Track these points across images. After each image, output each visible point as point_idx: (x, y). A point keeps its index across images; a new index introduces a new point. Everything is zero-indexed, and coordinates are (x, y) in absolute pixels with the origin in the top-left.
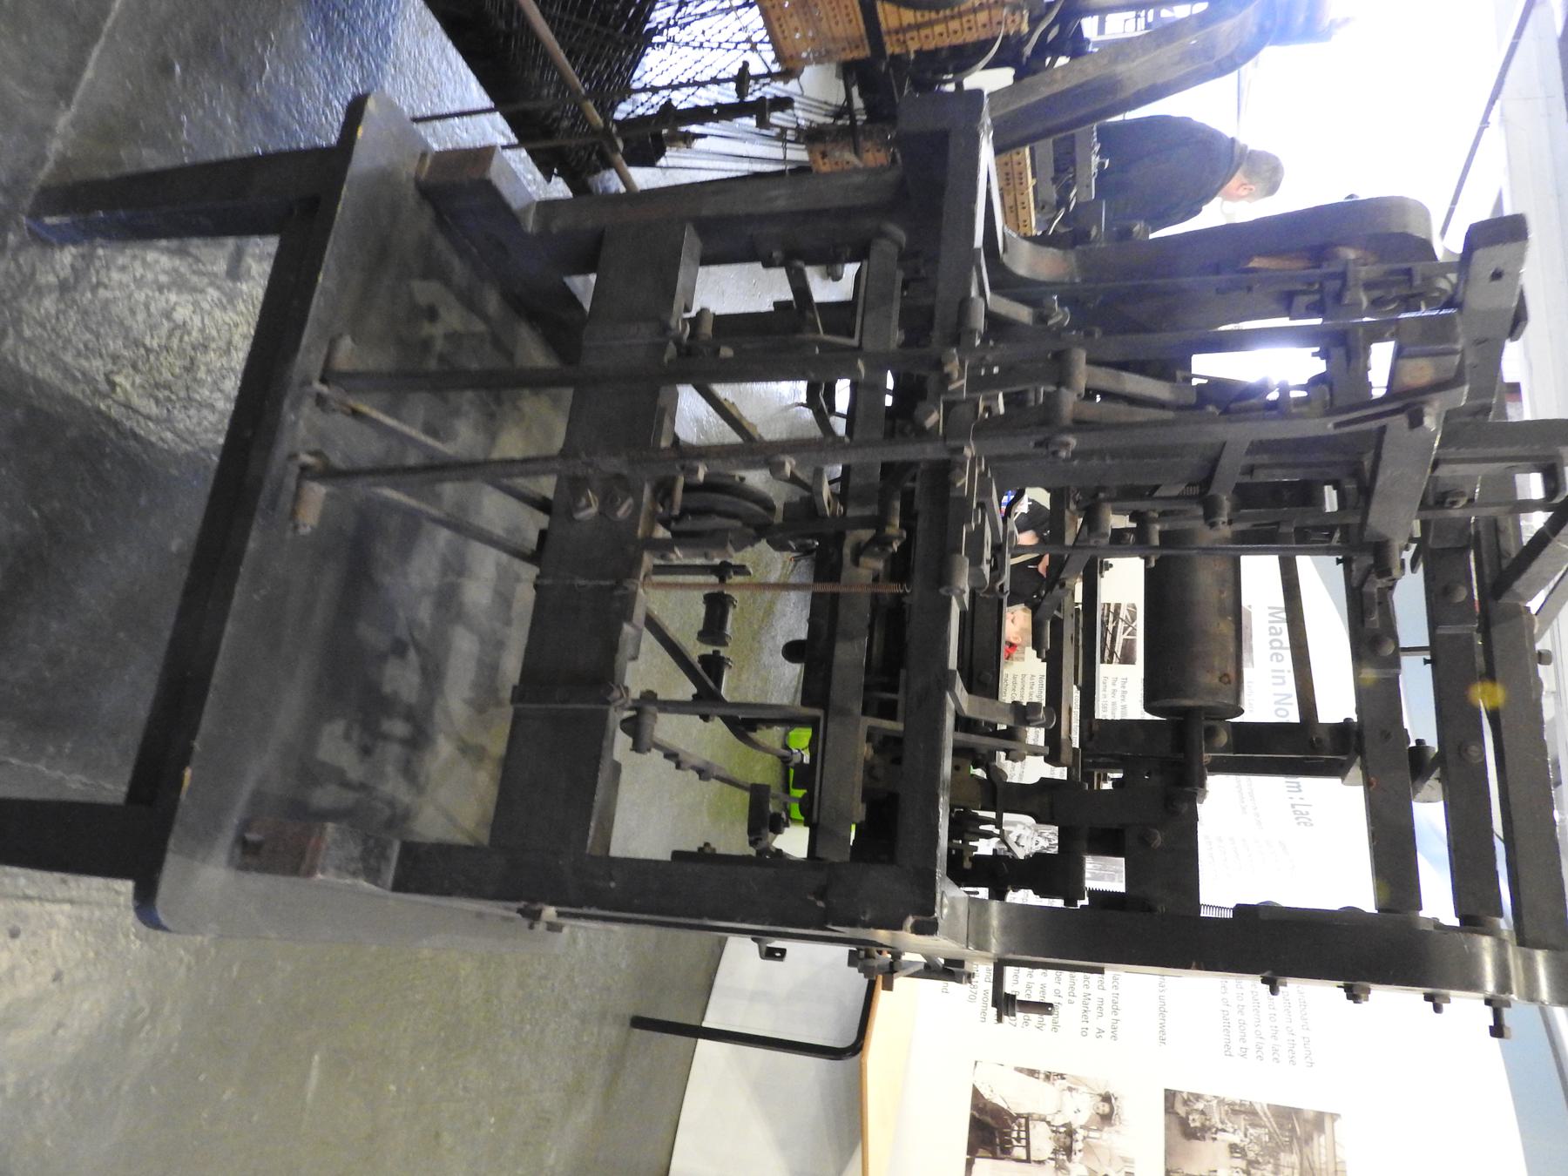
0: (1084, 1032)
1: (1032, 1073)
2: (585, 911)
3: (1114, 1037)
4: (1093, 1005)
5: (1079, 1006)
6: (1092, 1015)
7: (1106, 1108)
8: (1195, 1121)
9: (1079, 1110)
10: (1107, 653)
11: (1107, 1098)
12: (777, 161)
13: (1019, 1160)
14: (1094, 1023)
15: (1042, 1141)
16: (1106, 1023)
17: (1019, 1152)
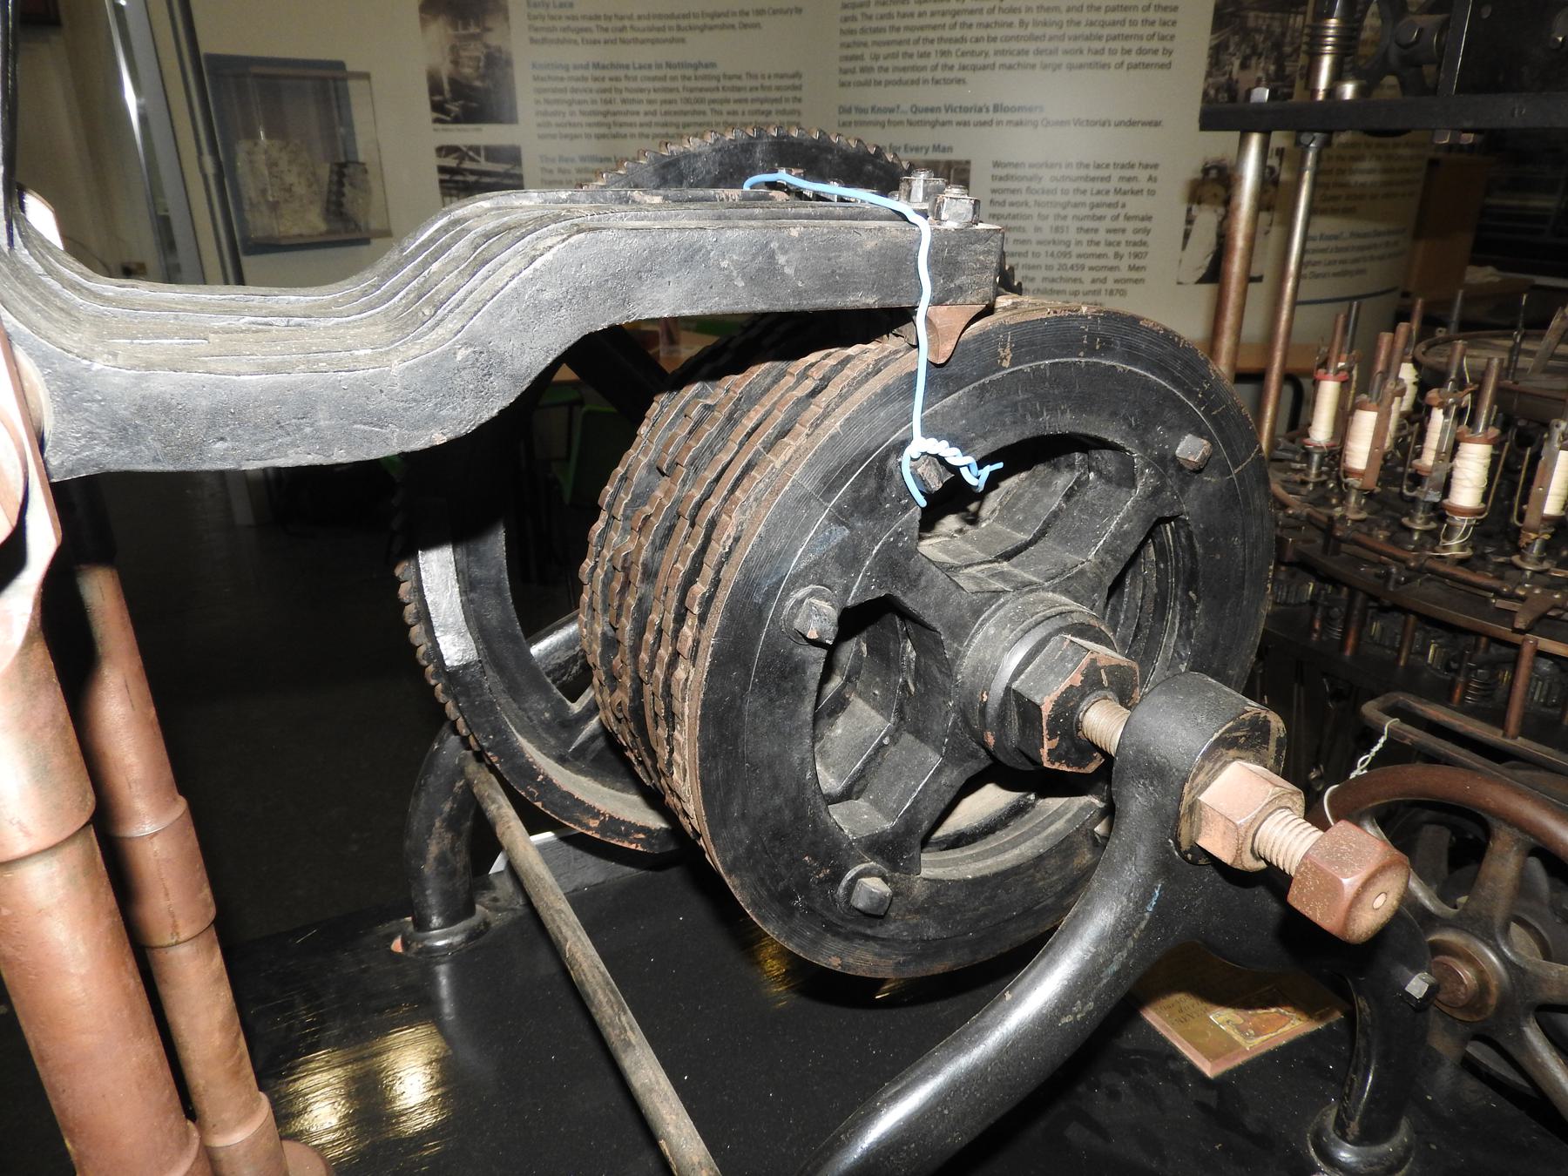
0: (1152, 193)
1: (1187, 235)
3: (1156, 166)
4: (1126, 186)
5: (1129, 199)
6: (1135, 186)
14: (1143, 184)
16: (1143, 175)
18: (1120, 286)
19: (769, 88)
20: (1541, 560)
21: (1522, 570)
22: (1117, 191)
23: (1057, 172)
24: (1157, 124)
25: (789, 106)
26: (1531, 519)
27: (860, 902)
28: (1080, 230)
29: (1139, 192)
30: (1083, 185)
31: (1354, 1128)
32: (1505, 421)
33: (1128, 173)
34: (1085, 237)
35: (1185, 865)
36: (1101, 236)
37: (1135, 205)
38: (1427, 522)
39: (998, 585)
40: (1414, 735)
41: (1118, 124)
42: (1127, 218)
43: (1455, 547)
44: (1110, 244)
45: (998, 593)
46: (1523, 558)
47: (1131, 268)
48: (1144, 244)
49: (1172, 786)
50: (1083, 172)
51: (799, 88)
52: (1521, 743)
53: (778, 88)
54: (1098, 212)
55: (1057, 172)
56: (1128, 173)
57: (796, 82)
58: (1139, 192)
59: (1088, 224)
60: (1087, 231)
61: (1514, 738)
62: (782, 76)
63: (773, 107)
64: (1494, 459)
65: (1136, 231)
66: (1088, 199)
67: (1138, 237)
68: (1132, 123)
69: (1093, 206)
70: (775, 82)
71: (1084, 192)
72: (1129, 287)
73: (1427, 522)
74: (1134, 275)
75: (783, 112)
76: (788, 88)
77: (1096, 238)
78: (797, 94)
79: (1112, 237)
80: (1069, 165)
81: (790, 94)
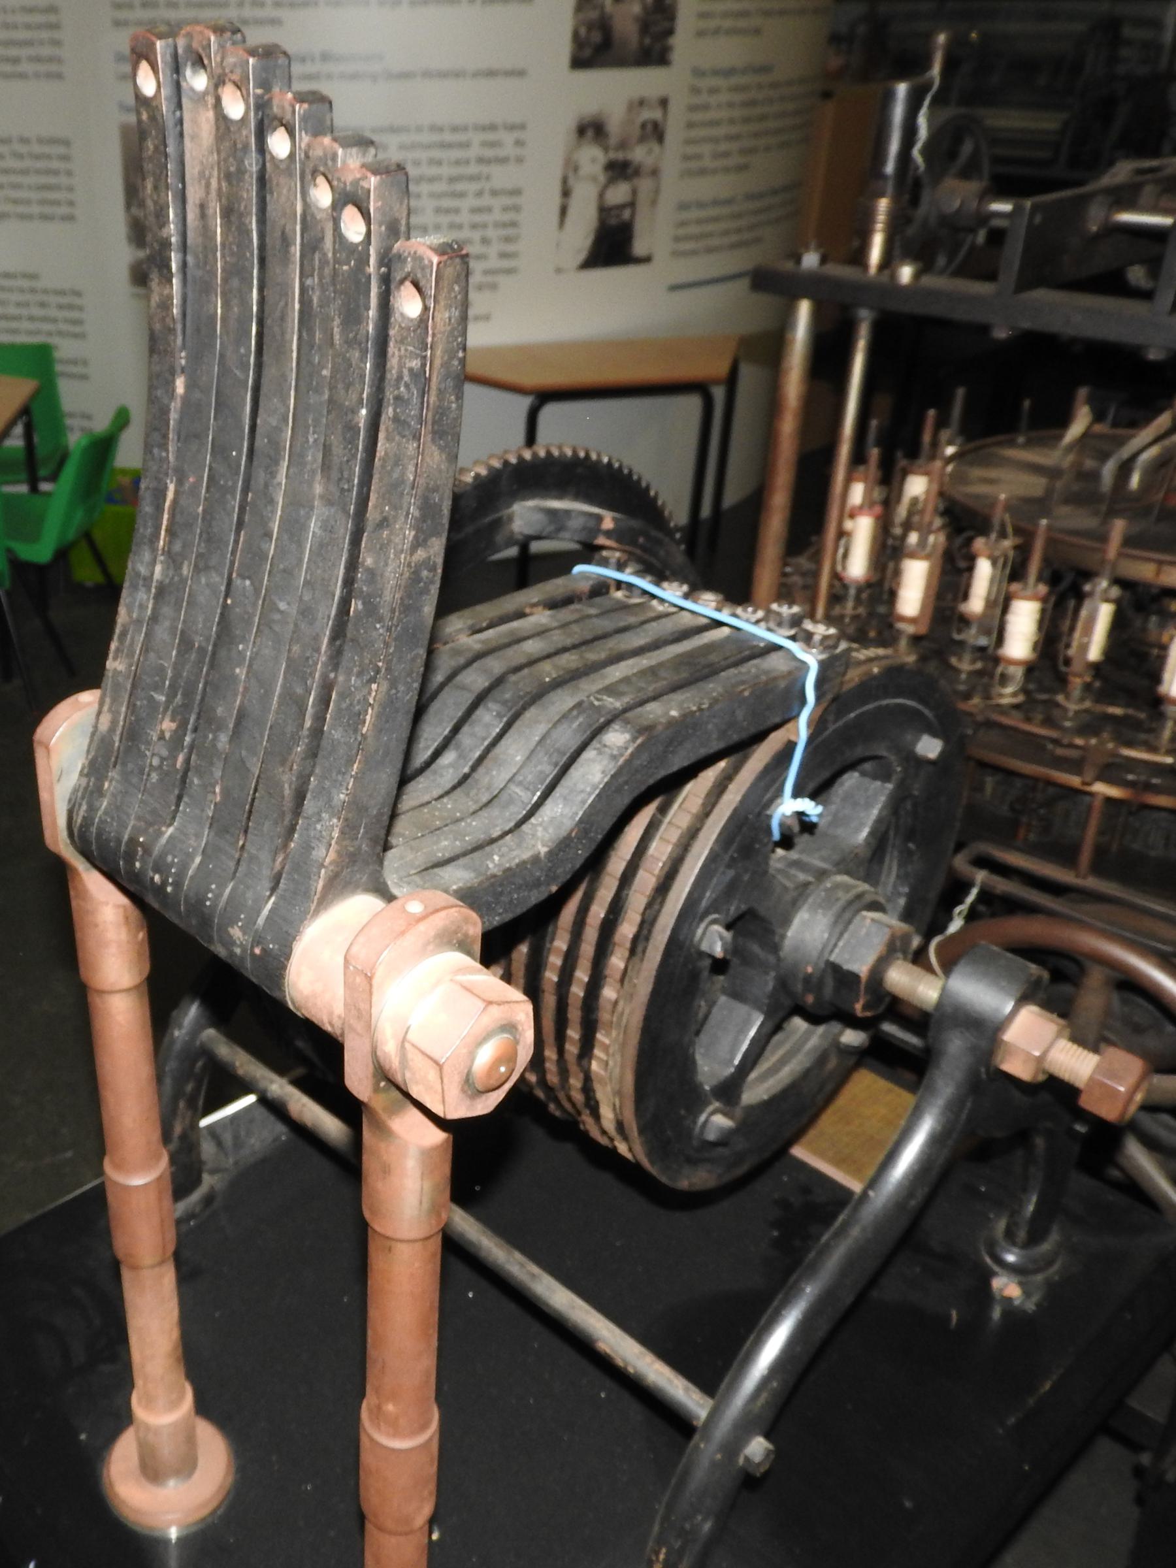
0: (520, 160)
1: (564, 211)
2: (763, 1322)
3: (522, 127)
4: (489, 153)
5: (496, 170)
6: (501, 153)
7: (590, 133)
8: (597, 37)
9: (592, 158)
10: (573, 1033)
11: (581, 131)
12: (574, 1105)
13: (633, 215)
14: (509, 150)
15: (619, 194)
16: (508, 138)
17: (626, 214)
18: (490, 279)
19: (15, 27)
20: (1082, 699)
21: (1065, 710)
22: (481, 160)
23: (405, 138)
24: (520, 73)
25: (46, 51)
26: (1077, 666)
27: (711, 1136)
28: (438, 210)
29: (503, 161)
30: (437, 154)
31: (1022, 1234)
32: (1053, 577)
33: (490, 136)
34: (444, 220)
35: (989, 1083)
36: (465, 218)
37: (501, 177)
38: (973, 661)
39: (802, 877)
40: (1003, 886)
41: (476, 74)
42: (494, 193)
43: (1008, 694)
44: (474, 226)
45: (806, 885)
46: (1068, 697)
47: (503, 255)
48: (514, 224)
49: (986, 1032)
50: (435, 138)
51: (55, 26)
52: (1091, 882)
53: (28, 27)
54: (460, 187)
55: (405, 138)
56: (490, 136)
57: (52, 18)
58: (503, 161)
59: (447, 203)
60: (448, 211)
61: (1085, 877)
62: (31, 10)
63: (24, 52)
64: (1043, 611)
65: (505, 209)
66: (446, 171)
67: (507, 217)
68: (491, 73)
69: (452, 180)
70: (20, 18)
71: (439, 163)
72: (502, 280)
73: (973, 661)
74: (506, 264)
75: (38, 59)
76: (40, 27)
77: (457, 219)
78: (56, 35)
79: (478, 218)
80: (419, 129)
81: (45, 35)
